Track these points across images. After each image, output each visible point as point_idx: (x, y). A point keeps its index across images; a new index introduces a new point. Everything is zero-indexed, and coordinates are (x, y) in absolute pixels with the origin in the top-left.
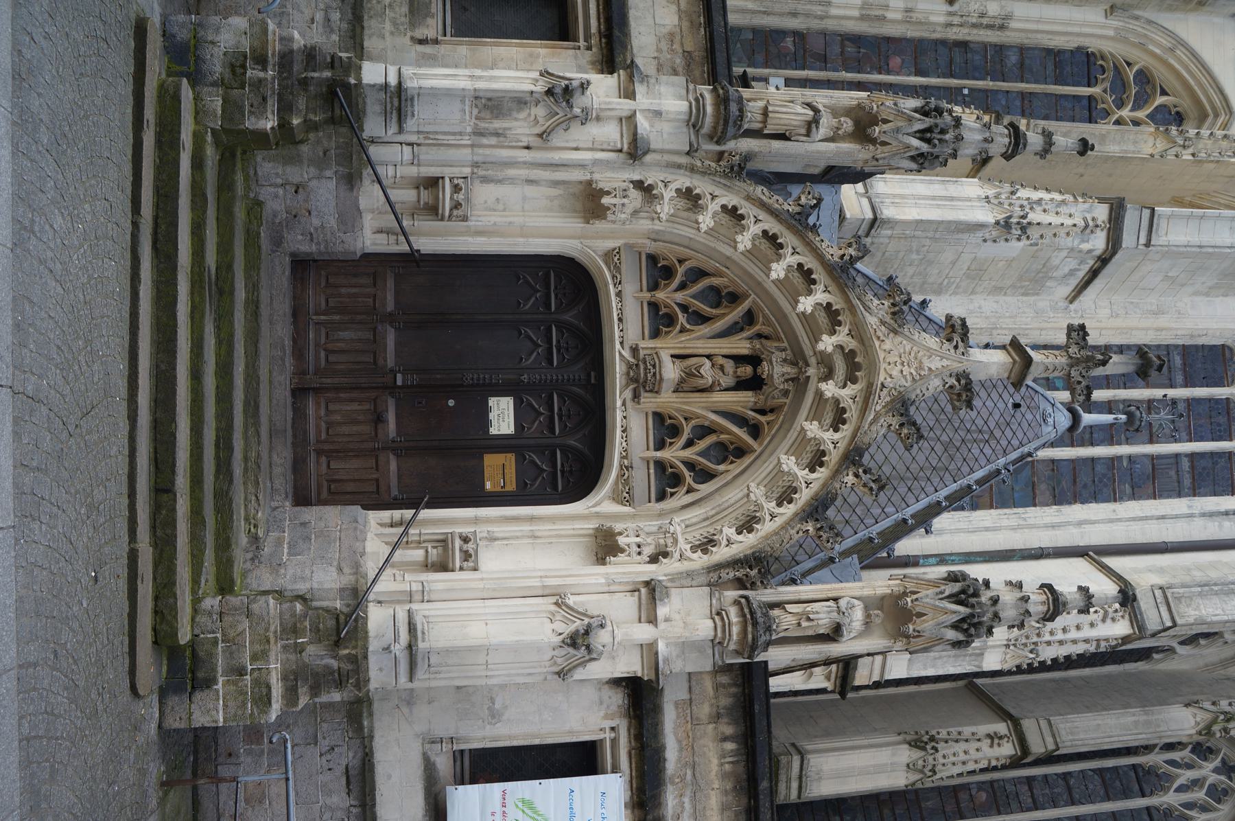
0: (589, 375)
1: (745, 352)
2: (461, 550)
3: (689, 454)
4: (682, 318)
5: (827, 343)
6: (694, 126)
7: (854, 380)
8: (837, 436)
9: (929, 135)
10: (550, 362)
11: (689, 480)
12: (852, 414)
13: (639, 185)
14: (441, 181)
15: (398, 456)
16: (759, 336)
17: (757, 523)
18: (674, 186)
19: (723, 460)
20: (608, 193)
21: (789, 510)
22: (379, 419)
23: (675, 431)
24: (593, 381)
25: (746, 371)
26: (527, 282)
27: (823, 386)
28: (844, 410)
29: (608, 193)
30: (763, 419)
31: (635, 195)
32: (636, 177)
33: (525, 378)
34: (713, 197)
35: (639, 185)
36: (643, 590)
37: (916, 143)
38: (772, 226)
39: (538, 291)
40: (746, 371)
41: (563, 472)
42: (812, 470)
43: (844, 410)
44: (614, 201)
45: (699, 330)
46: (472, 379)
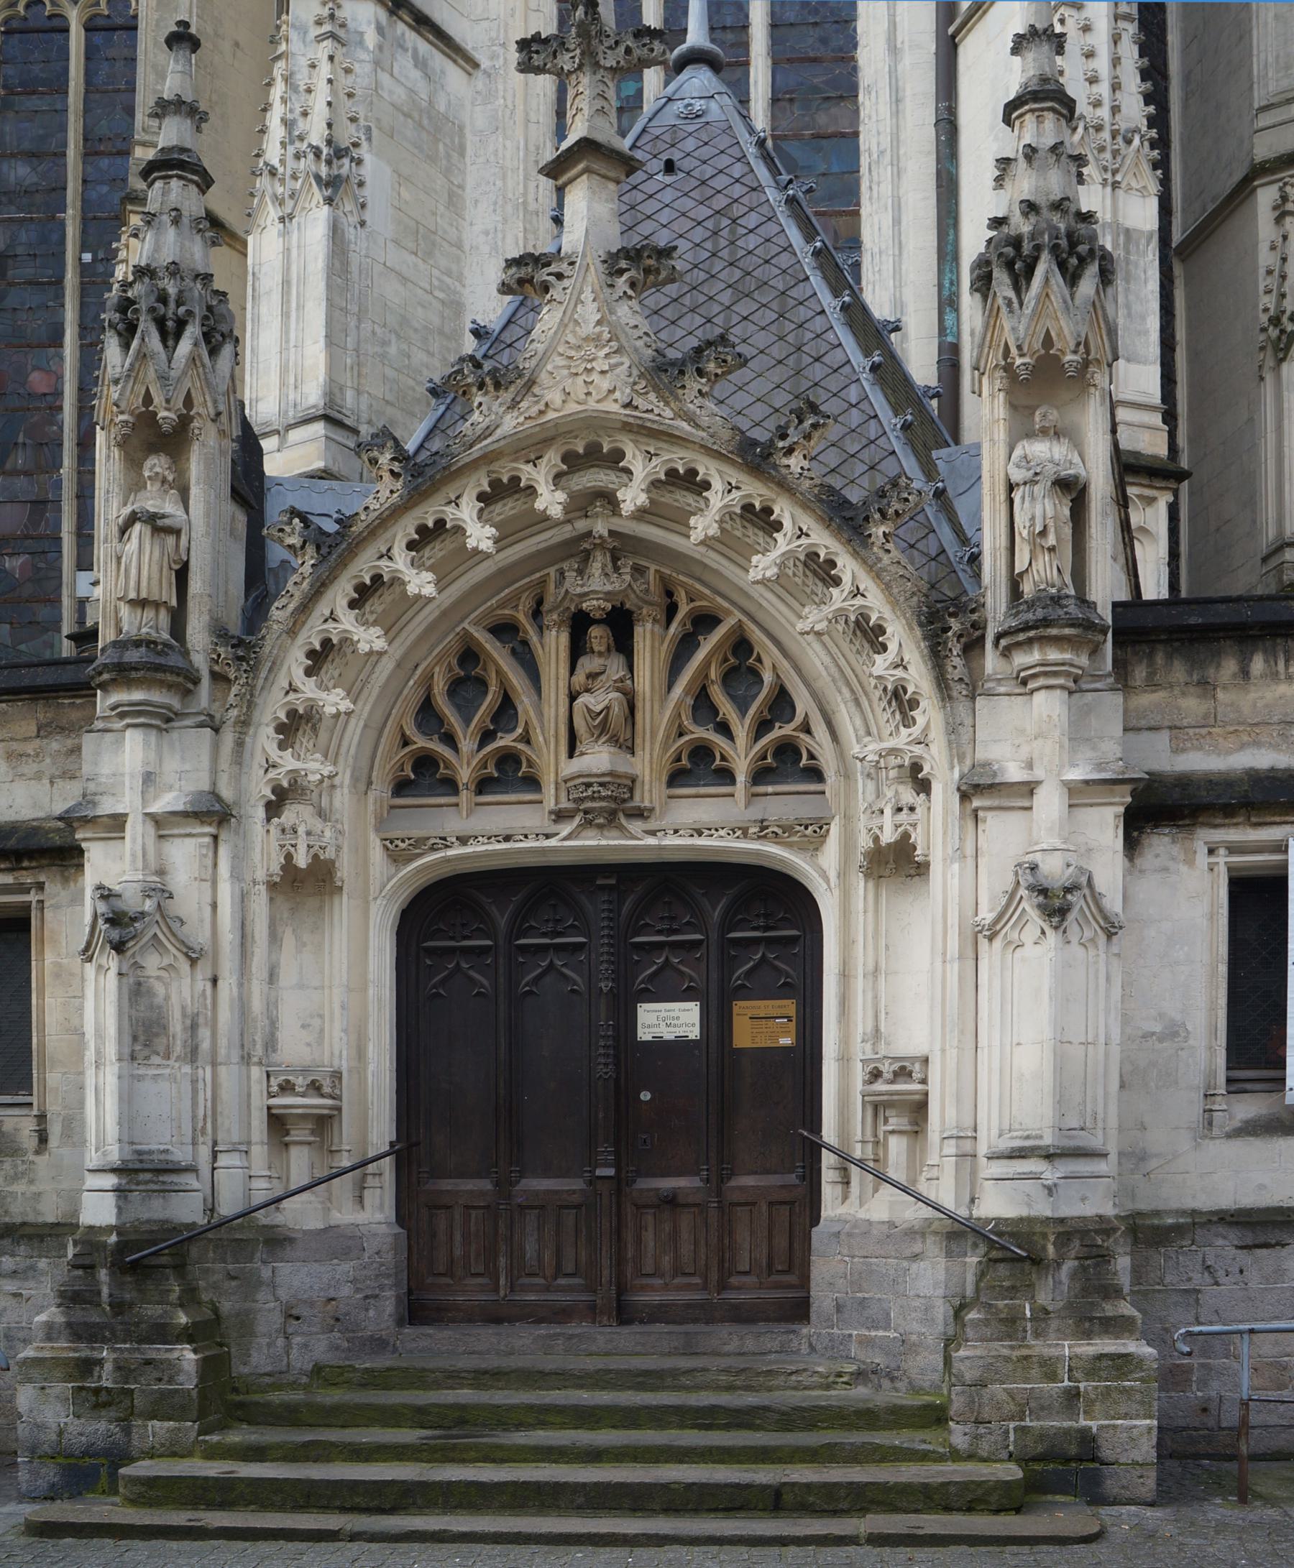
0: (602, 887)
1: (564, 638)
2: (892, 1082)
3: (741, 730)
4: (505, 740)
5: (550, 500)
6: (169, 720)
7: (619, 455)
8: (717, 484)
9: (170, 324)
10: (578, 947)
11: (788, 730)
12: (679, 459)
13: (273, 809)
14: (274, 1111)
15: (733, 1174)
16: (537, 614)
17: (867, 619)
18: (274, 754)
19: (756, 675)
20: (289, 857)
21: (847, 566)
22: (671, 1201)
23: (702, 752)
24: (613, 882)
25: (598, 636)
26: (443, 982)
27: (627, 508)
28: (672, 473)
29: (289, 857)
30: (683, 609)
31: (289, 815)
32: (260, 813)
33: (605, 986)
34: (292, 689)
35: (273, 809)
36: (976, 803)
37: (184, 347)
38: (341, 592)
39: (458, 963)
40: (598, 636)
41: (767, 928)
42: (778, 526)
43: (672, 473)
44: (302, 848)
45: (526, 712)
46: (606, 1065)
